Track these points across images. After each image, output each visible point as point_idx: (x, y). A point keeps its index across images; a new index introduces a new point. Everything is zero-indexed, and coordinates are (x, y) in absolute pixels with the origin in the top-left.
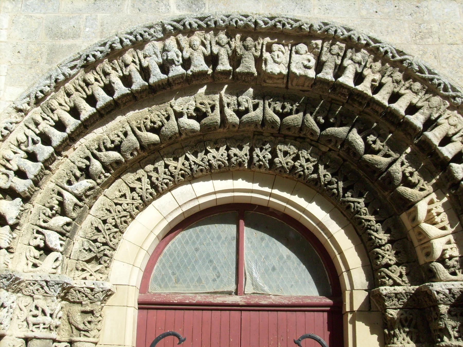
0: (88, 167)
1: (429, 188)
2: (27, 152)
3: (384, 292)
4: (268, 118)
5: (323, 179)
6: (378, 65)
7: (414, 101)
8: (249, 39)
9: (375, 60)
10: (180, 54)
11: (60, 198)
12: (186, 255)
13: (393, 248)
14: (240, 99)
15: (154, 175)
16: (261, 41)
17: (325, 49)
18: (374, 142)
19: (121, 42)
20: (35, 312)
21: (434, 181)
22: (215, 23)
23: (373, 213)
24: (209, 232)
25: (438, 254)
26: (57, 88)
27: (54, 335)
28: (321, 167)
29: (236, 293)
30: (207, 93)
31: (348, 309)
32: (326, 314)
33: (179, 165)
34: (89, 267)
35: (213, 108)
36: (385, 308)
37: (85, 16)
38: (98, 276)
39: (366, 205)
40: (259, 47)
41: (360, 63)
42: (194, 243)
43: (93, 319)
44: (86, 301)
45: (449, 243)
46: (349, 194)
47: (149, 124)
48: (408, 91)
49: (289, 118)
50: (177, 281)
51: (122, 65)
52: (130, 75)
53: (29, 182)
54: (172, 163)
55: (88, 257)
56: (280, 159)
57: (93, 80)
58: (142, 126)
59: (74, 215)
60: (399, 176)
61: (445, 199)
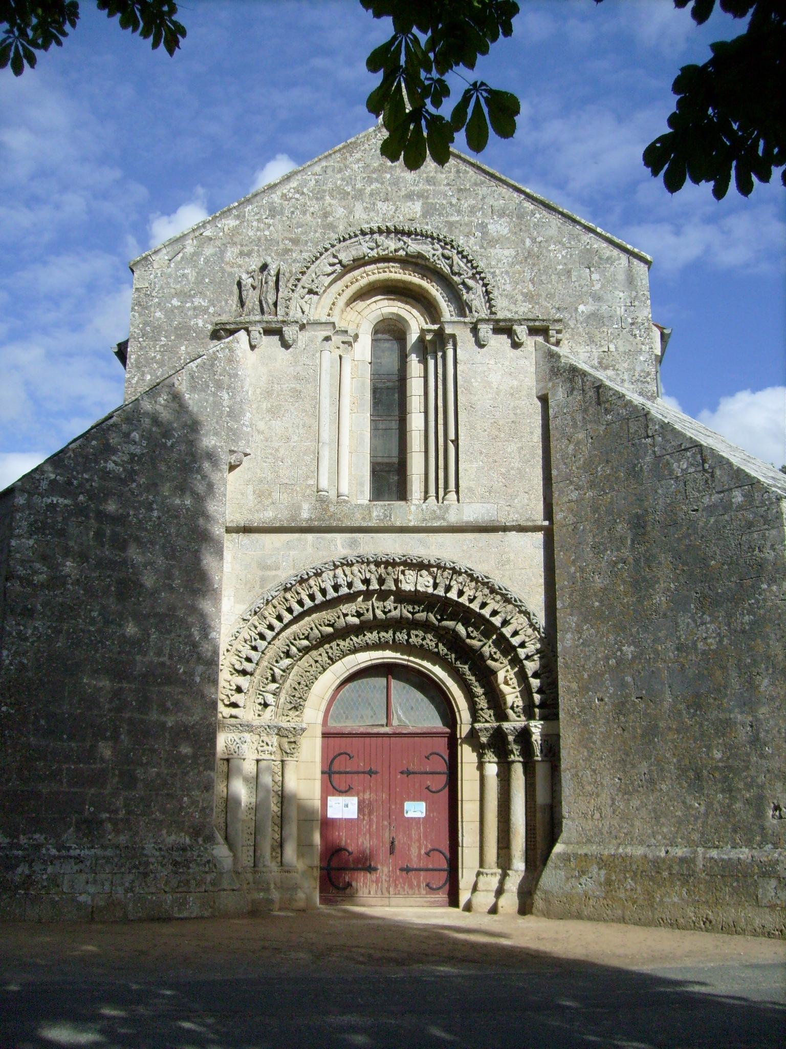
0: (288, 651)
1: (506, 662)
2: (251, 646)
3: (477, 728)
4: (404, 616)
5: (441, 652)
6: (473, 584)
7: (496, 609)
8: (390, 568)
9: (471, 581)
10: (345, 578)
11: (271, 672)
12: (352, 700)
13: (486, 698)
14: (385, 603)
15: (330, 651)
16: (397, 569)
17: (439, 574)
18: (472, 632)
19: (308, 574)
20: (262, 744)
21: (510, 657)
22: (367, 559)
23: (473, 675)
24: (368, 683)
25: (509, 704)
26: (267, 604)
27: (273, 757)
28: (440, 645)
29: (387, 725)
30: (364, 601)
31: (458, 736)
32: (446, 739)
33: (347, 645)
34: (291, 713)
35: (368, 610)
36: (479, 737)
37: (282, 553)
38: (297, 719)
39: (470, 670)
40: (396, 573)
41: (461, 583)
42: (358, 691)
43: (296, 746)
44: (290, 735)
45: (517, 697)
46: (458, 662)
47: (327, 622)
48: (492, 601)
49: (417, 615)
50: (347, 718)
51: (308, 587)
52: (313, 594)
53: (253, 665)
54: (342, 643)
55: (290, 707)
56: (413, 640)
57: (290, 598)
58: (322, 624)
59: (281, 682)
60: (487, 654)
61: (516, 669)
